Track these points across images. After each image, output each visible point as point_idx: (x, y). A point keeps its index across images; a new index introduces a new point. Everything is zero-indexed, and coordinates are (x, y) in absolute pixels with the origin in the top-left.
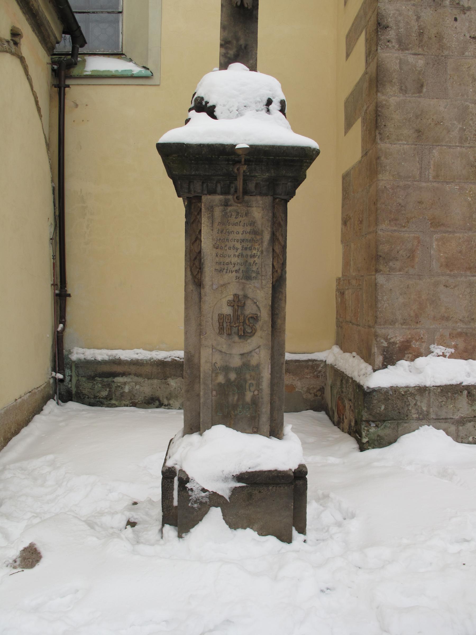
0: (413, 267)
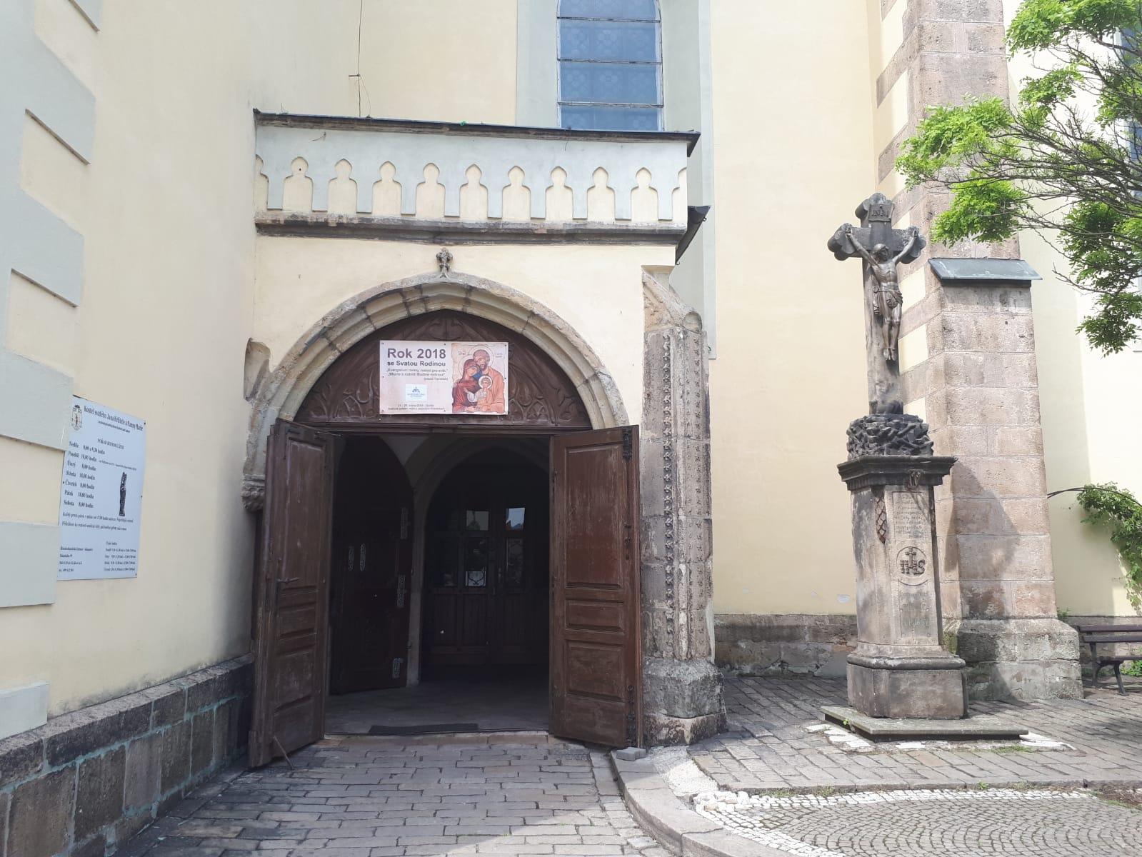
0: (987, 528)
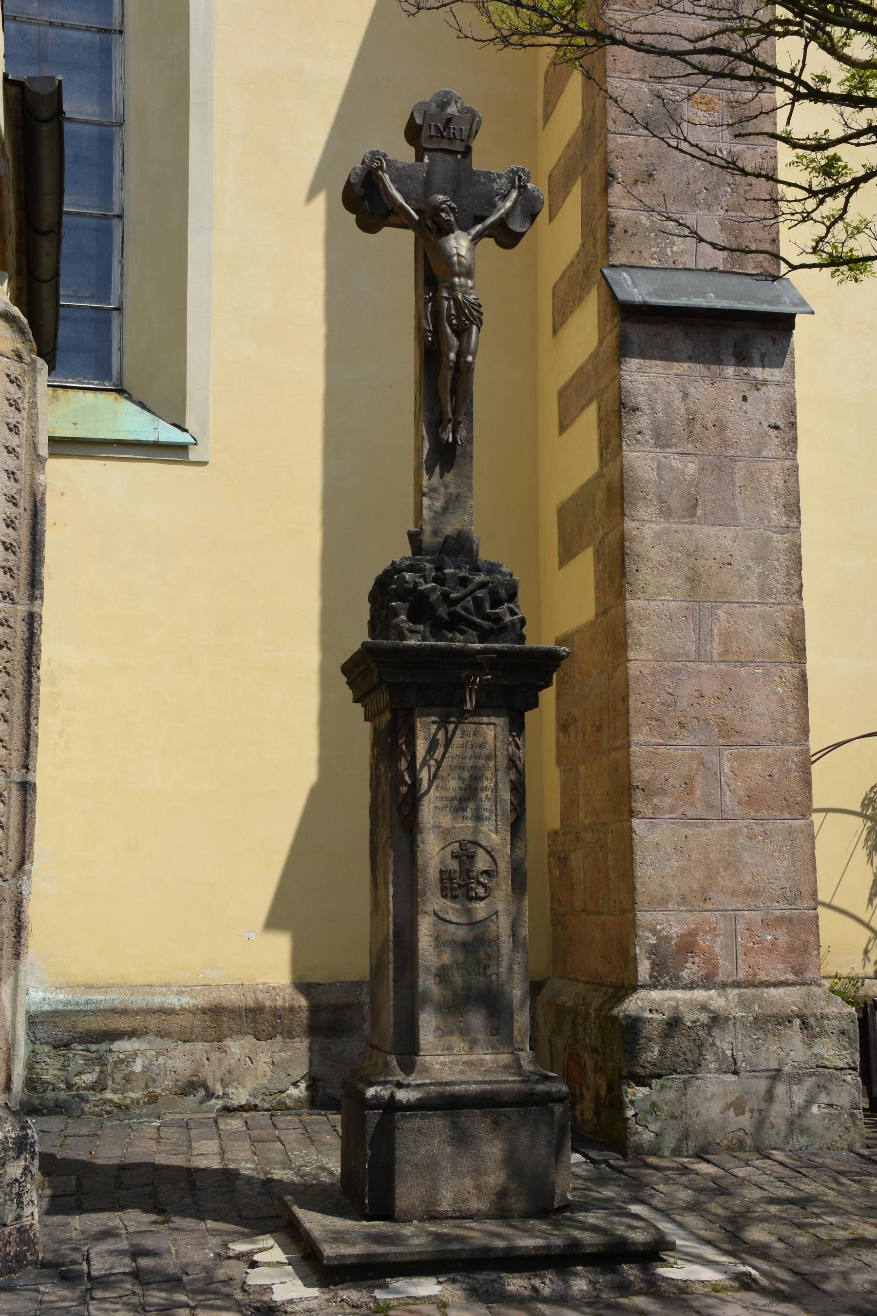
0: (693, 805)
